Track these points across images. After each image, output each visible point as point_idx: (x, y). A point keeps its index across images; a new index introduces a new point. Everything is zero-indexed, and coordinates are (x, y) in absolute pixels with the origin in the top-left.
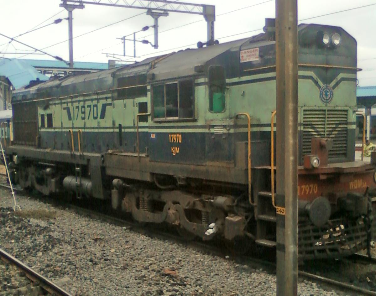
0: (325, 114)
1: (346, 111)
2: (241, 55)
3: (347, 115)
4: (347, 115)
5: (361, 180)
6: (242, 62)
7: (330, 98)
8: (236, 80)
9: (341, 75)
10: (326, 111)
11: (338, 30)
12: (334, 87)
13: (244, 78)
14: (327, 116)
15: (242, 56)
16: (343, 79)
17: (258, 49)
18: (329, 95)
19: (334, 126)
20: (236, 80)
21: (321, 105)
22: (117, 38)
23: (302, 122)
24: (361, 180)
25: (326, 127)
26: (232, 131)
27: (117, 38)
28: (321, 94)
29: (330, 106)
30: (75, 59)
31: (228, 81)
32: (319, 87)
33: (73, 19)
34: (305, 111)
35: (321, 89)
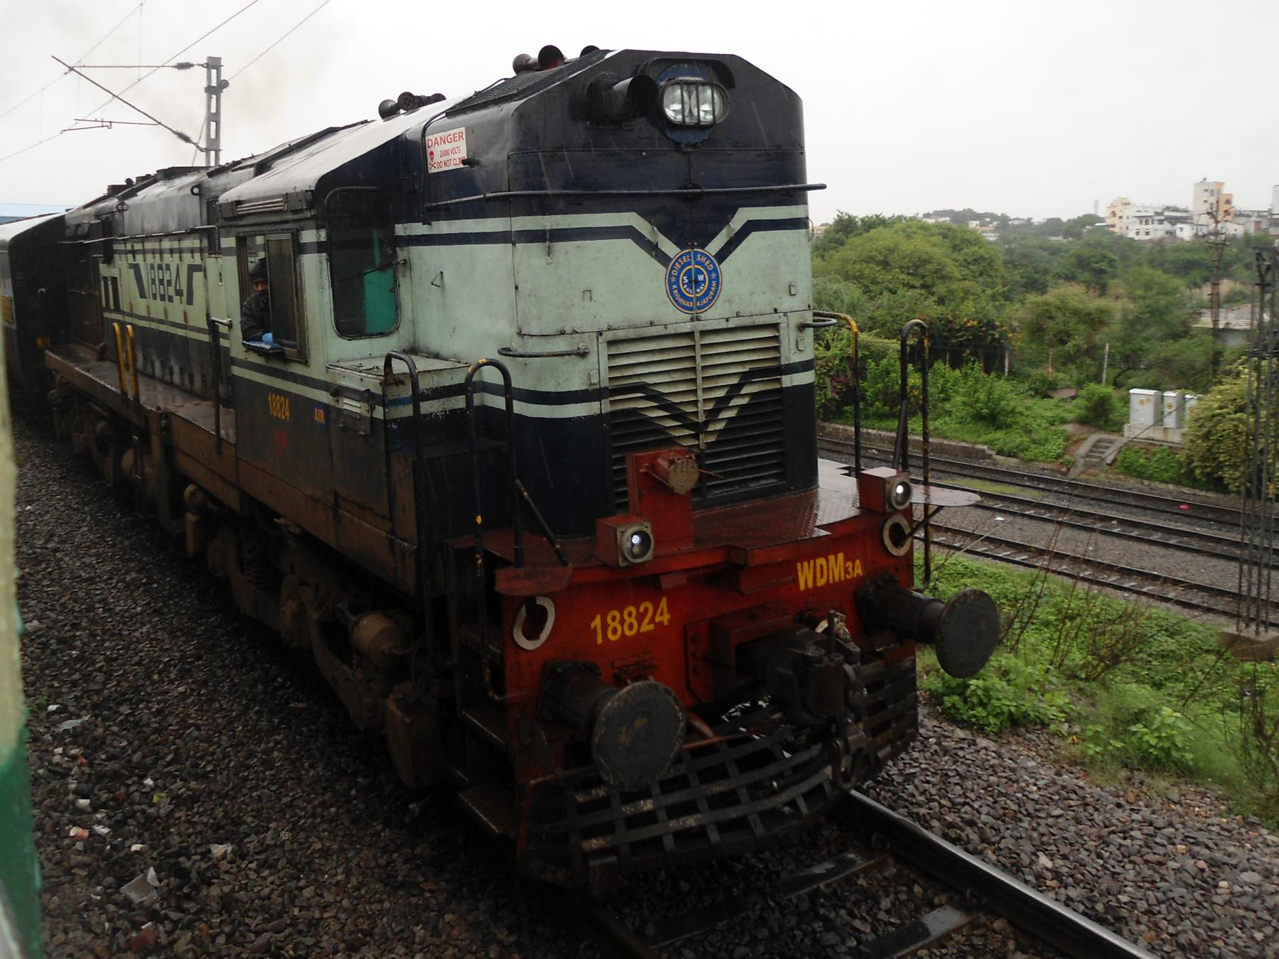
0: (693, 358)
1: (775, 326)
2: (428, 151)
3: (776, 338)
4: (776, 338)
5: (841, 556)
6: (433, 170)
7: (706, 294)
8: (419, 229)
9: (743, 215)
10: (697, 335)
11: (723, 71)
12: (722, 255)
13: (443, 227)
14: (700, 363)
15: (432, 153)
16: (752, 226)
17: (463, 129)
18: (704, 282)
19: (735, 381)
20: (419, 229)
21: (679, 320)
22: (823, 187)
23: (605, 384)
24: (841, 556)
25: (700, 399)
26: (379, 413)
27: (823, 187)
28: (672, 283)
29: (714, 316)
30: (810, 193)
31: (400, 230)
32: (662, 258)
33: (1029, 219)
34: (611, 343)
35: (672, 268)
